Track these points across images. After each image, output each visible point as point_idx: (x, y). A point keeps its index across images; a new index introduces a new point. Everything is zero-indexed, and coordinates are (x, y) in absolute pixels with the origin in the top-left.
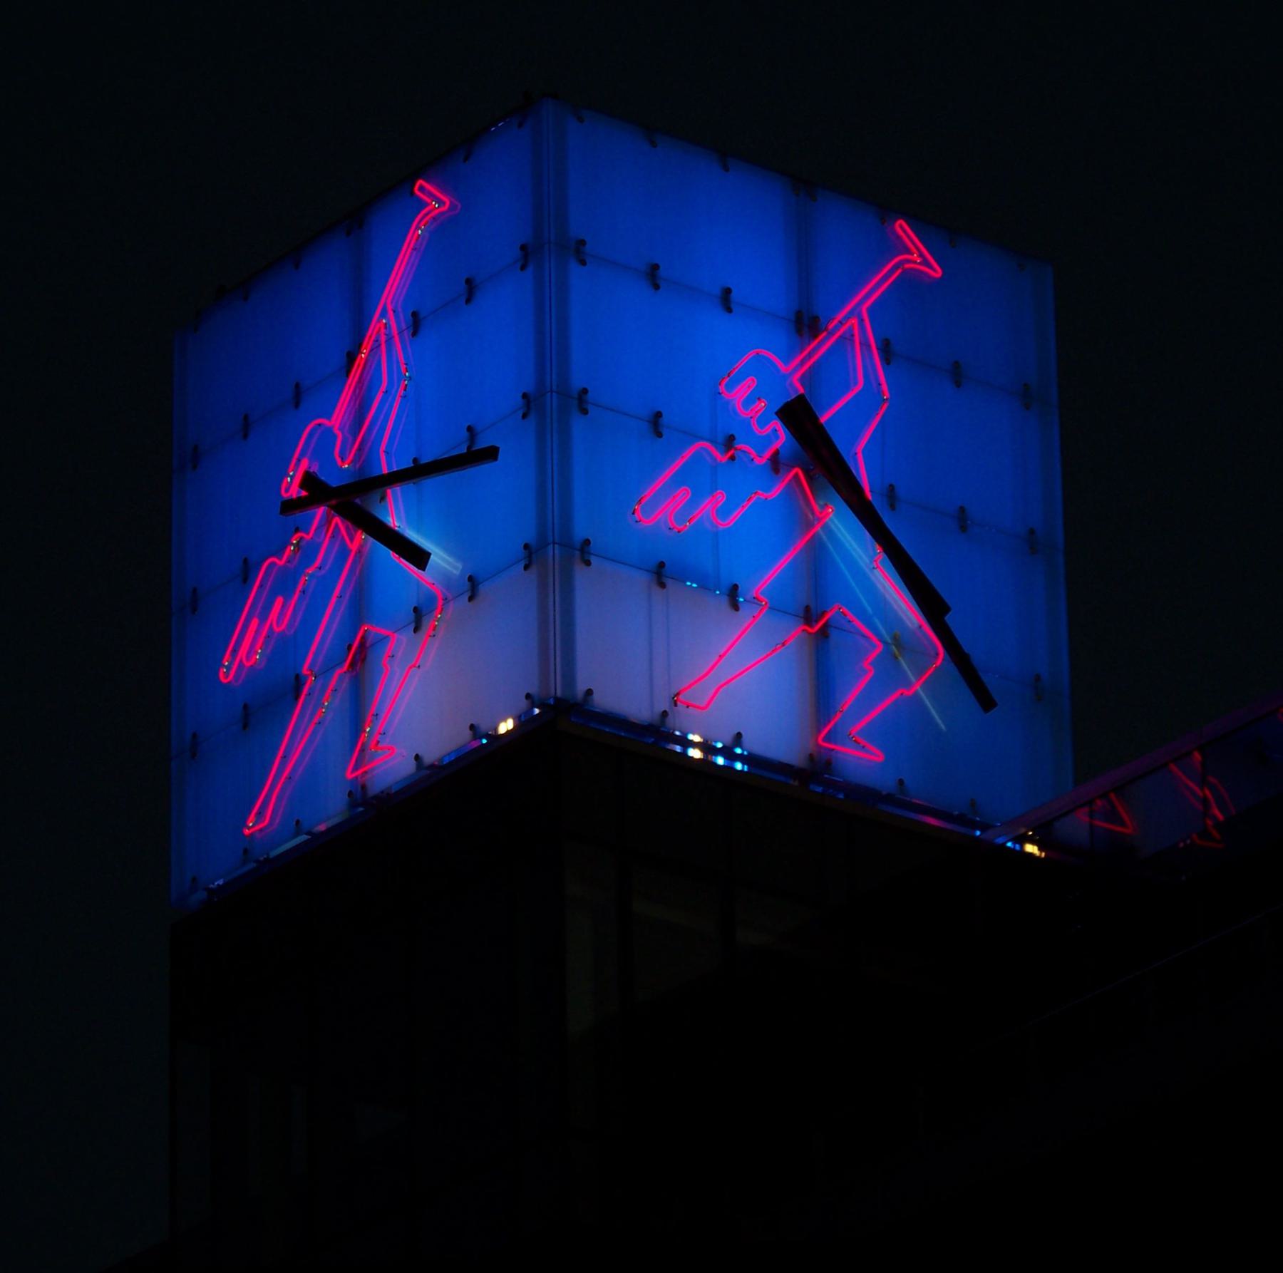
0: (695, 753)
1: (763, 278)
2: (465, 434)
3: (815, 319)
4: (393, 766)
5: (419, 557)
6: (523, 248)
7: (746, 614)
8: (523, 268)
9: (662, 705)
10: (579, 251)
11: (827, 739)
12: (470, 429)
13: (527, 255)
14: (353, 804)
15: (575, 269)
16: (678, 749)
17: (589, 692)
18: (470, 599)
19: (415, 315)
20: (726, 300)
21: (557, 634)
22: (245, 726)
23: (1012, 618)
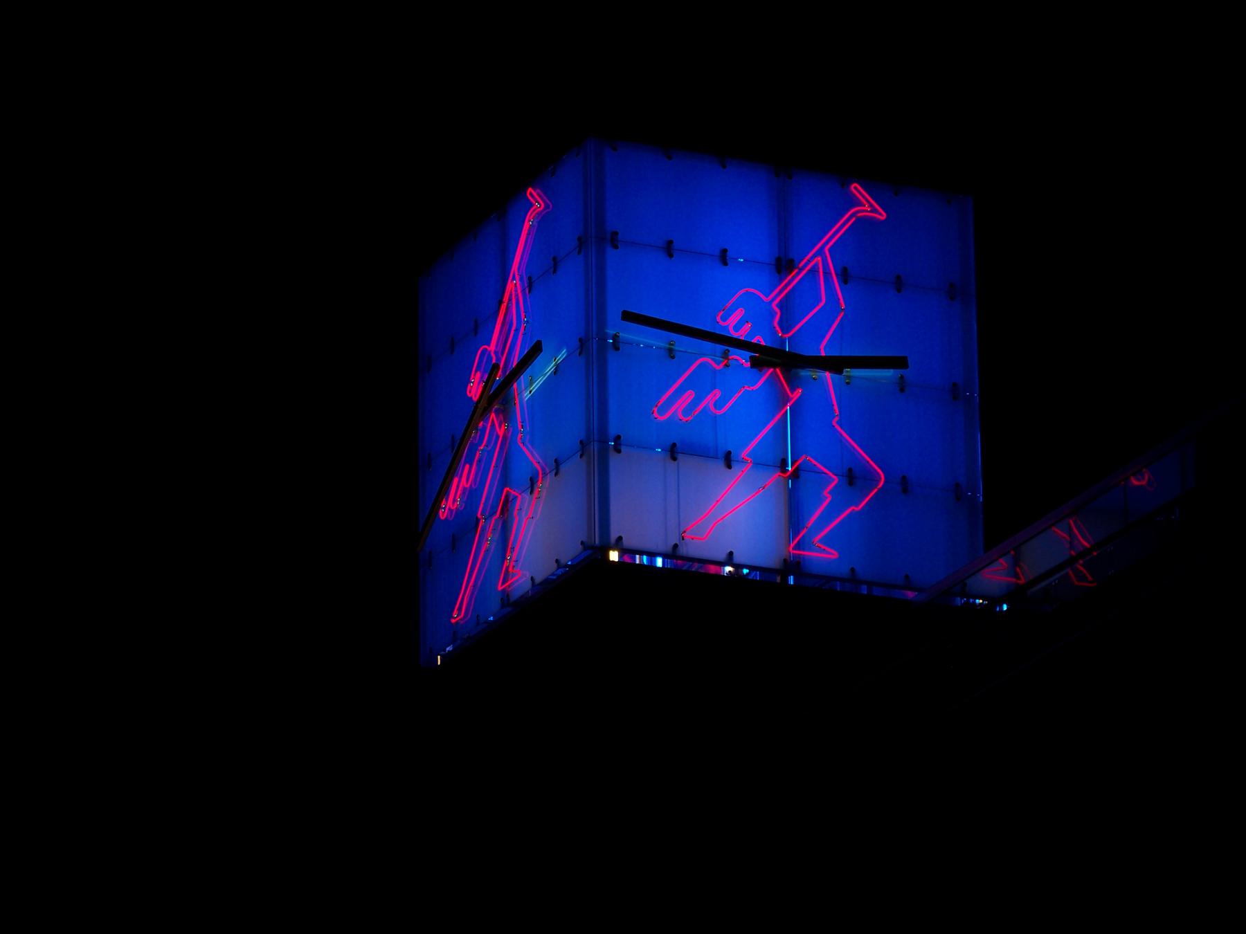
1: (750, 237)
3: (792, 261)
4: (521, 583)
7: (737, 469)
9: (674, 540)
11: (798, 547)
13: (582, 243)
14: (503, 606)
15: (610, 251)
18: (556, 474)
20: (723, 258)
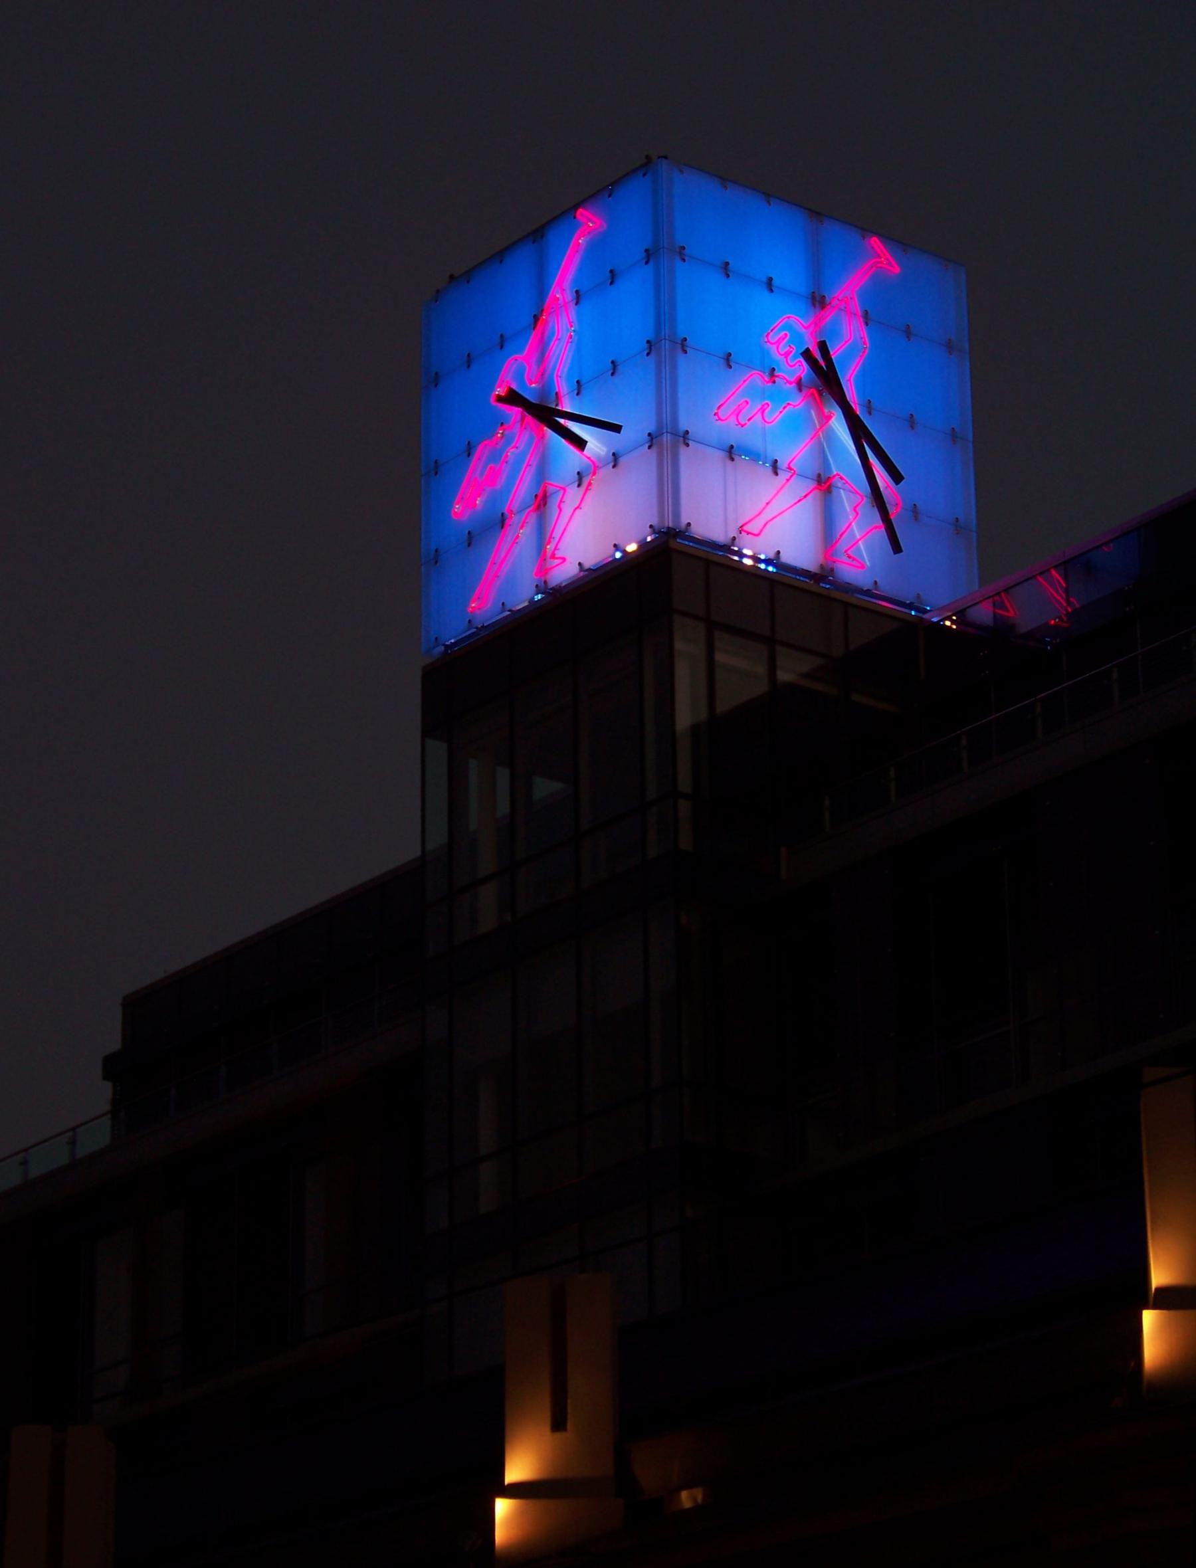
0: (748, 562)
1: (791, 272)
2: (611, 365)
4: (564, 574)
5: (580, 443)
6: (646, 251)
7: (783, 476)
8: (647, 263)
10: (681, 252)
12: (613, 362)
13: (649, 255)
15: (679, 265)
16: (736, 558)
17: (689, 524)
19: (577, 292)
20: (769, 284)
21: (668, 488)
22: (469, 545)
23: (936, 481)
